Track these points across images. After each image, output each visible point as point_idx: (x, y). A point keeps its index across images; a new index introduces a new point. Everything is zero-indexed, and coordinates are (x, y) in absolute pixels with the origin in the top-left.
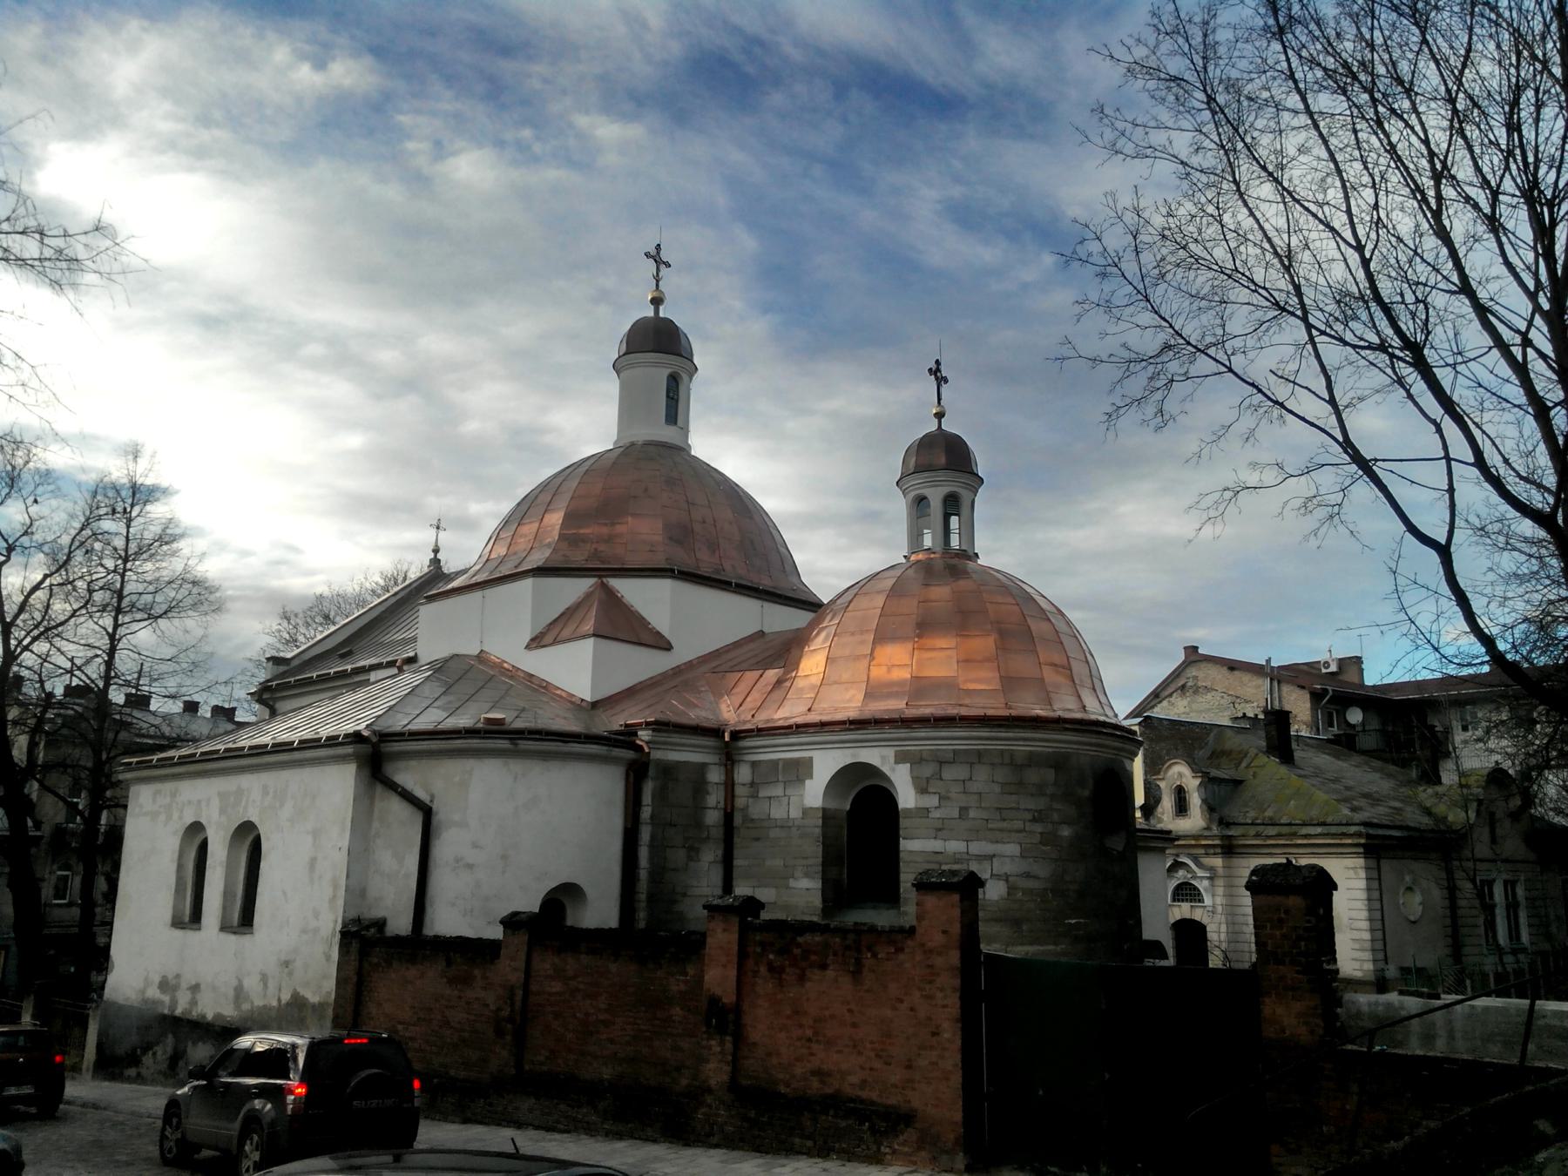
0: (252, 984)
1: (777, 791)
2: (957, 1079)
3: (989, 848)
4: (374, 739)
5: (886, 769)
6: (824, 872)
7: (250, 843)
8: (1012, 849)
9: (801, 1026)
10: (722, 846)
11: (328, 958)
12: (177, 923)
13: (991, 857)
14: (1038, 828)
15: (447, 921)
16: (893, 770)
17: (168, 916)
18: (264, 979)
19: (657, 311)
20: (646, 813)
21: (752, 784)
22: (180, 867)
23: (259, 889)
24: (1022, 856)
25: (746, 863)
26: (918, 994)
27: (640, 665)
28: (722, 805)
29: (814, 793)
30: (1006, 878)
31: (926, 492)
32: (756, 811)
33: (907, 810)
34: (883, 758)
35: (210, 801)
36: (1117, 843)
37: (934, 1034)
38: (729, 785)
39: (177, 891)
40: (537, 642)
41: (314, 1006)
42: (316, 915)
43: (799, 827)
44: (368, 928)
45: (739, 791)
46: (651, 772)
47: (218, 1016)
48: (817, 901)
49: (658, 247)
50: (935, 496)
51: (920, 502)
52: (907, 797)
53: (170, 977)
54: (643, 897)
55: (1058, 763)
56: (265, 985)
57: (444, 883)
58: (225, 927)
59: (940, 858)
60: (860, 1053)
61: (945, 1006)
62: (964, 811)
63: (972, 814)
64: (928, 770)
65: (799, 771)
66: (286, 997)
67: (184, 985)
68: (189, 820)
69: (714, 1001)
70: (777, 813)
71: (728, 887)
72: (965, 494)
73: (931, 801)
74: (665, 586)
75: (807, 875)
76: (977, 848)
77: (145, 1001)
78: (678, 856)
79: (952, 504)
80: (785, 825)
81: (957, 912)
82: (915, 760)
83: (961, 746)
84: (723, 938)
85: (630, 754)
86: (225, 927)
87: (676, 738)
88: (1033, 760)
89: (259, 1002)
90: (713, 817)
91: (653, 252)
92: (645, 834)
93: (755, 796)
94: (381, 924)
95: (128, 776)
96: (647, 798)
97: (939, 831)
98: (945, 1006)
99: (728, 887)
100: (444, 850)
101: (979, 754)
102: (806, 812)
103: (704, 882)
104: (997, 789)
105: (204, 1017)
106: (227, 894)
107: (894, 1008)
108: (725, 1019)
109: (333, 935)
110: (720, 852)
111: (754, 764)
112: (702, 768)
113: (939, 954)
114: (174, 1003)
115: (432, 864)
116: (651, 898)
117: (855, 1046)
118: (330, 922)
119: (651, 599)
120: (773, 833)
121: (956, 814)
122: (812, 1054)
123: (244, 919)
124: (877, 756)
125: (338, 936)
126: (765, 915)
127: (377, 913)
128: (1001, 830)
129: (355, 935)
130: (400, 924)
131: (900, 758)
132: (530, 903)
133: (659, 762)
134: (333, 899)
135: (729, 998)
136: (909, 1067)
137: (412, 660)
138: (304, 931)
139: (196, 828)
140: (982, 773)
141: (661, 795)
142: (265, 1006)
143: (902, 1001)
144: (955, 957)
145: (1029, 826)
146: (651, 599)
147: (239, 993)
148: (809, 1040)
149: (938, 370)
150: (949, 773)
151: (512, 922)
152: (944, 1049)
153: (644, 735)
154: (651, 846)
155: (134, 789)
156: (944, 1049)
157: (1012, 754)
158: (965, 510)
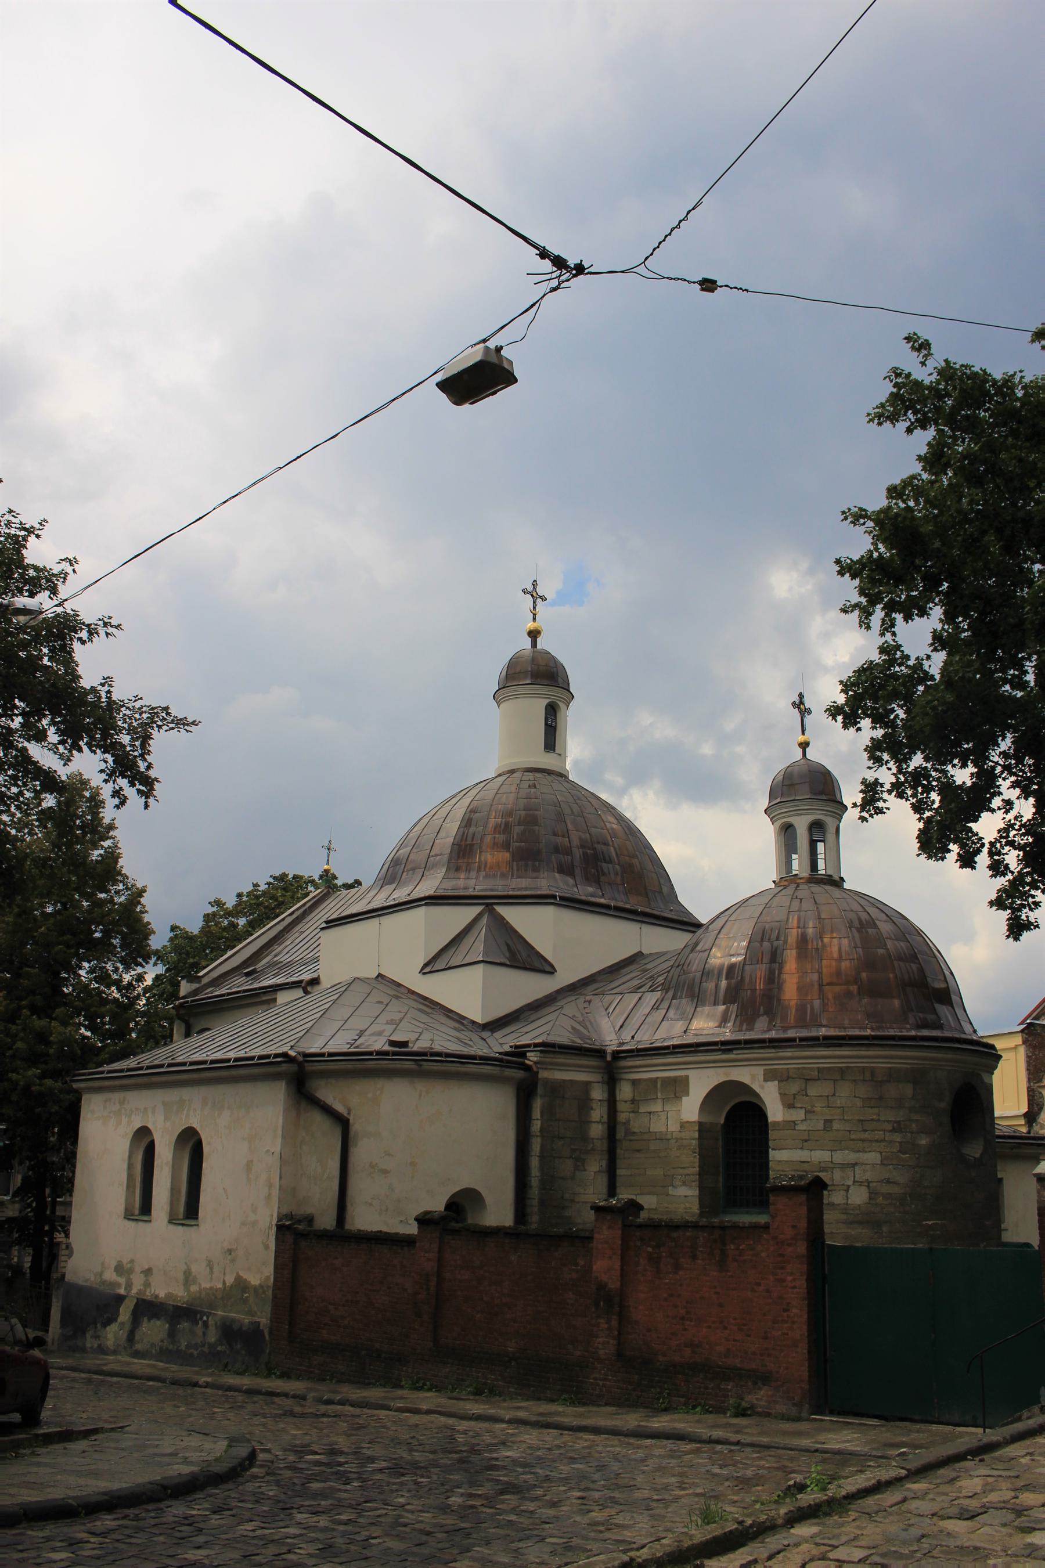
0: (198, 1269)
1: (657, 1107)
2: (803, 1348)
3: (850, 1157)
4: (301, 1059)
5: (756, 1087)
6: (701, 1181)
7: (192, 1145)
8: (873, 1157)
9: (676, 1307)
10: (606, 1157)
11: (267, 1247)
12: (129, 1215)
13: (854, 1165)
14: (897, 1137)
15: (365, 1218)
16: (762, 1087)
17: (121, 1209)
18: (210, 1265)
19: (534, 644)
20: (536, 1126)
21: (633, 1101)
22: (130, 1167)
23: (203, 1187)
24: (882, 1164)
25: (629, 1173)
26: (771, 1278)
27: (524, 988)
28: (605, 1119)
29: (689, 1109)
30: (868, 1183)
31: (793, 820)
32: (636, 1125)
33: (775, 1123)
34: (753, 1077)
35: (163, 1115)
36: (974, 1150)
37: (785, 1310)
38: (612, 1103)
39: (128, 1187)
40: (429, 968)
41: (256, 1289)
42: (254, 1209)
43: (677, 1139)
44: (299, 1222)
45: (621, 1107)
46: (540, 1090)
47: (169, 1295)
48: (695, 1209)
49: (535, 584)
50: (801, 824)
51: (787, 831)
52: (775, 1112)
53: (125, 1262)
54: (535, 1202)
55: (917, 1077)
56: (211, 1269)
57: (361, 1187)
58: (172, 1220)
59: (806, 1166)
60: (725, 1328)
61: (794, 1287)
62: (828, 1122)
63: (836, 1126)
64: (794, 1088)
65: (678, 1088)
66: (230, 1280)
67: (138, 1269)
68: (138, 1125)
69: (601, 1286)
70: (657, 1126)
71: (612, 1192)
72: (830, 822)
73: (798, 1115)
74: (548, 913)
75: (684, 1184)
76: (839, 1157)
77: (104, 1283)
78: (566, 1167)
79: (817, 828)
80: (663, 1138)
81: (804, 1211)
82: (782, 1078)
83: (826, 1064)
84: (608, 1235)
85: (520, 1074)
86: (172, 1220)
87: (560, 1059)
88: (893, 1076)
89: (206, 1285)
90: (597, 1130)
91: (530, 588)
92: (536, 1146)
93: (635, 1112)
94: (310, 1220)
95: (82, 1085)
96: (536, 1113)
97: (806, 1141)
98: (794, 1287)
99: (612, 1192)
100: (362, 1153)
101: (842, 1071)
102: (683, 1125)
103: (590, 1188)
104: (859, 1103)
105: (157, 1296)
106: (174, 1190)
107: (753, 1290)
108: (612, 1303)
109: (270, 1228)
110: (604, 1163)
111: (635, 1083)
112: (588, 1084)
113: (789, 1245)
114: (129, 1286)
115: (350, 1166)
116: (542, 1203)
117: (721, 1322)
118: (267, 1217)
119: (536, 925)
120: (653, 1146)
121: (820, 1125)
122: (685, 1330)
123: (190, 1210)
124: (748, 1074)
125: (274, 1229)
126: (644, 1215)
127: (309, 1210)
128: (863, 1140)
129: (288, 1227)
130: (326, 1221)
131: (769, 1076)
132: (438, 1205)
133: (546, 1081)
134: (269, 1197)
135: (614, 1284)
136: (765, 1338)
137: (315, 982)
138: (243, 1224)
139: (143, 1132)
140: (845, 1090)
141: (548, 1112)
142: (211, 1288)
143: (759, 1284)
144: (802, 1248)
145: (888, 1136)
146: (536, 925)
147: (188, 1278)
148: (683, 1318)
149: (802, 702)
150: (813, 1090)
151: (424, 1220)
152: (793, 1323)
153: (532, 1057)
154: (542, 1157)
155: (85, 1098)
156: (793, 1323)
157: (873, 1071)
158: (830, 836)
